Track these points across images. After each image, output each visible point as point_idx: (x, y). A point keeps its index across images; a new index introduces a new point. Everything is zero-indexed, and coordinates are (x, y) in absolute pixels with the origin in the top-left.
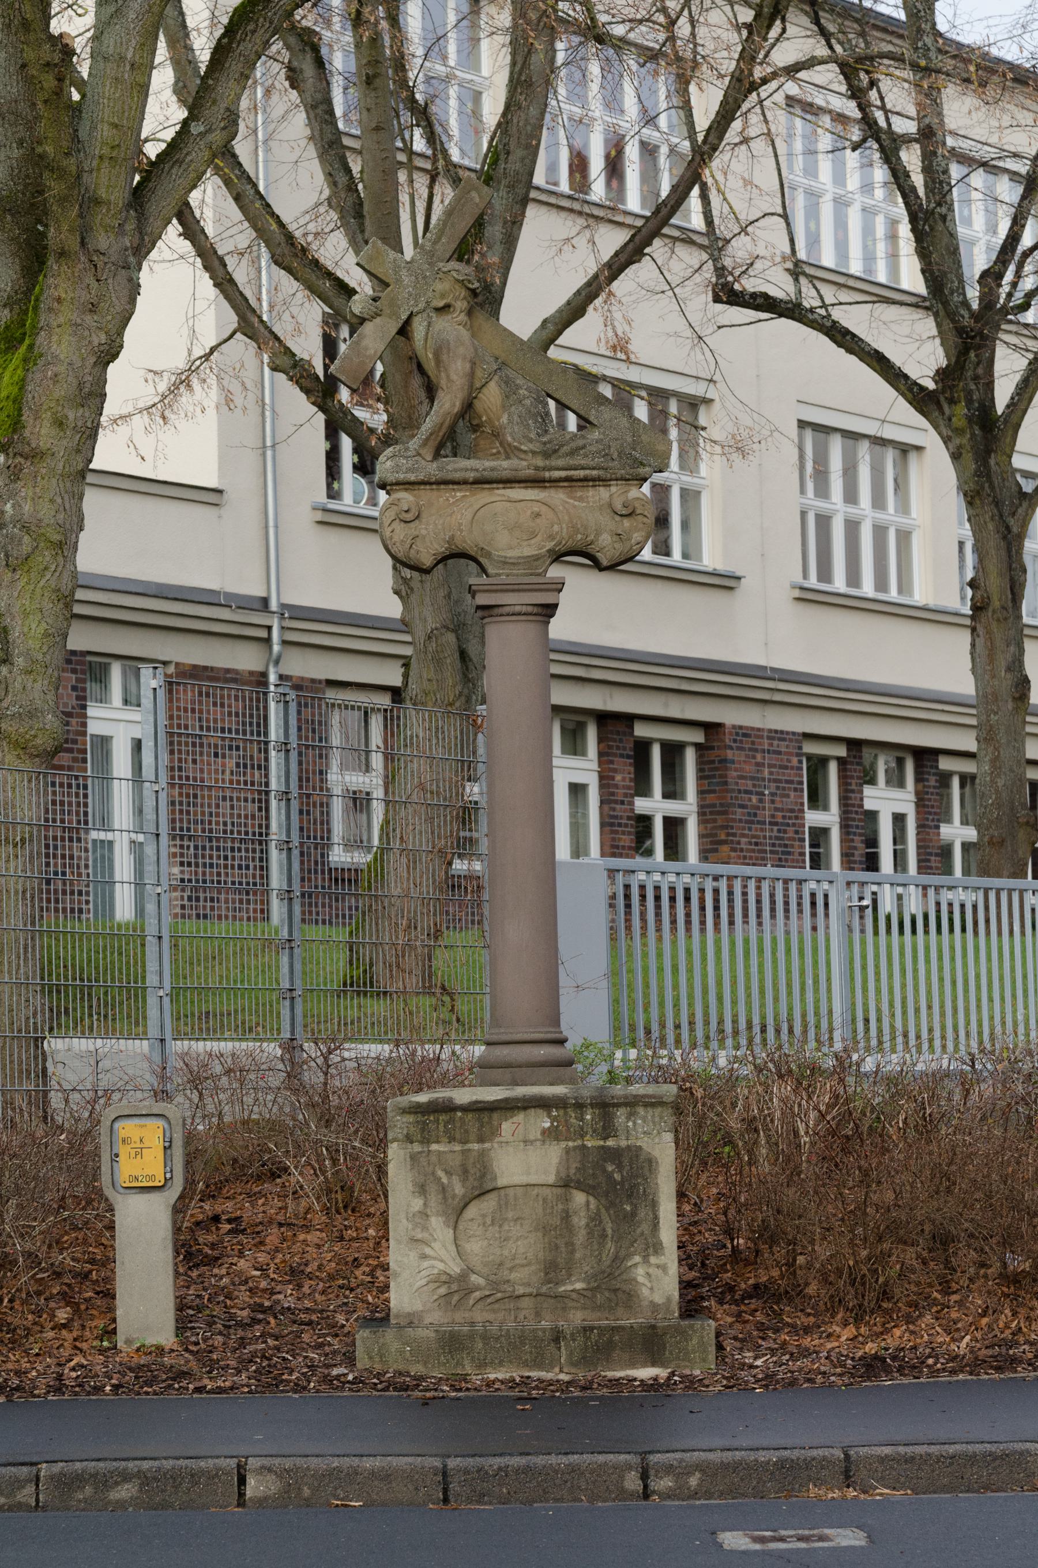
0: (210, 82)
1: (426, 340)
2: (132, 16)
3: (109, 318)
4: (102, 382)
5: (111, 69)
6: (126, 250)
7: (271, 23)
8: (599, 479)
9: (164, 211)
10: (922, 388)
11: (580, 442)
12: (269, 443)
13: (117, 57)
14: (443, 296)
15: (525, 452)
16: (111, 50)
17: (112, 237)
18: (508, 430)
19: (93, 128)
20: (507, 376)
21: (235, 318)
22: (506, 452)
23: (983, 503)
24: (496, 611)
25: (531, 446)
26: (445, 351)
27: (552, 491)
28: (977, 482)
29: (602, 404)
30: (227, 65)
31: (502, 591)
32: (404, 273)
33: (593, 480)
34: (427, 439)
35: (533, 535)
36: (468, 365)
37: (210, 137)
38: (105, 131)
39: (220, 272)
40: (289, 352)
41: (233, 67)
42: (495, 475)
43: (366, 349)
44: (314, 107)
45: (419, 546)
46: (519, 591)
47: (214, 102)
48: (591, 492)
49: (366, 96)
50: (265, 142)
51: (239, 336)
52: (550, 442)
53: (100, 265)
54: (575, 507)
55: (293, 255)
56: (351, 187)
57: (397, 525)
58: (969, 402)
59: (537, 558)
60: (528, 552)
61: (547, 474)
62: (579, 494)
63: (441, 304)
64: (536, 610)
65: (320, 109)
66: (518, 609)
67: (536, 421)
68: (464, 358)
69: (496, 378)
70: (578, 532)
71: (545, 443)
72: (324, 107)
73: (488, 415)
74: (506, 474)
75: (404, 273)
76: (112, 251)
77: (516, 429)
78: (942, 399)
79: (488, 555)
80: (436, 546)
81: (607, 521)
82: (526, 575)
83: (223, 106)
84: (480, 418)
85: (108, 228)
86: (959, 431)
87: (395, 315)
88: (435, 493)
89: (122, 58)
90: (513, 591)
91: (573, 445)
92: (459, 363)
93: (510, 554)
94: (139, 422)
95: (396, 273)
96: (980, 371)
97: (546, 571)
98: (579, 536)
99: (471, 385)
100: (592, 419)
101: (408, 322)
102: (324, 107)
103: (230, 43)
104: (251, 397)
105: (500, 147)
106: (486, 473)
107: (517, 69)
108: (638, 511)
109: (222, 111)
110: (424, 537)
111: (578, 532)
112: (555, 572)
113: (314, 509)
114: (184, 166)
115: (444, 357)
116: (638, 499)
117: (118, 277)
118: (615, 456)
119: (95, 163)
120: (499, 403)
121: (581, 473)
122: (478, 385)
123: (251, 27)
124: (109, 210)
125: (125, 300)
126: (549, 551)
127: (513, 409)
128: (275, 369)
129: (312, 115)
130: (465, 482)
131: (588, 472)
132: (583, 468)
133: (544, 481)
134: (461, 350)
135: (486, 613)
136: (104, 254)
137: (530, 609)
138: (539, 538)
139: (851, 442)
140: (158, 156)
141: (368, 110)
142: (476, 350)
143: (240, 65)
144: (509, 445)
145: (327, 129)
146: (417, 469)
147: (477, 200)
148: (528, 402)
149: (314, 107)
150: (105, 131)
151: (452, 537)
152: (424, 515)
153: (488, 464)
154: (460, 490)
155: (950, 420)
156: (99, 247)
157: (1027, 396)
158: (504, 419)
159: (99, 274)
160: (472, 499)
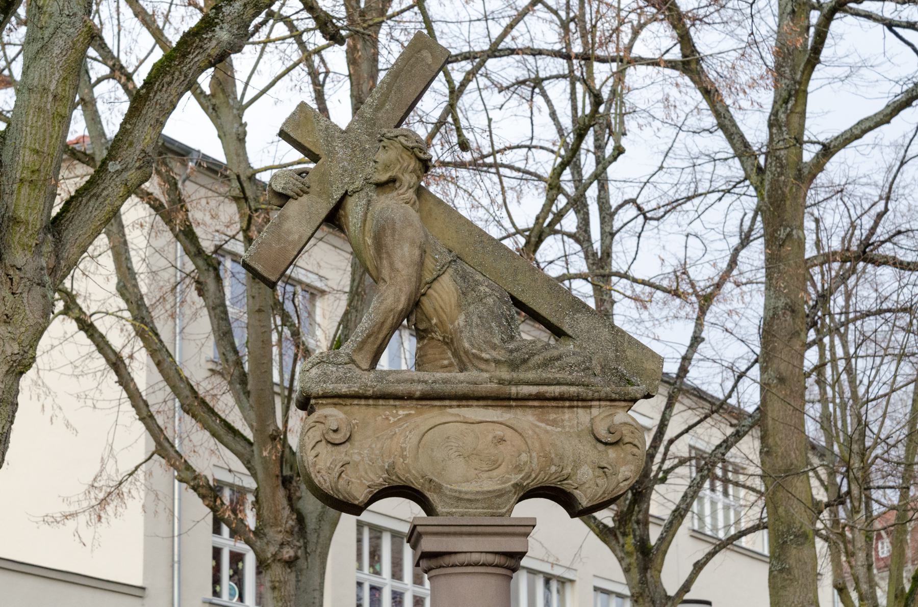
0: (128, 126)
1: (364, 221)
2: (57, 51)
3: (23, 329)
4: (14, 392)
5: (35, 100)
6: (42, 269)
7: (186, 76)
8: (579, 398)
9: (80, 240)
10: (605, 526)
11: (556, 353)
12: (176, 533)
13: (41, 89)
14: (387, 167)
15: (487, 361)
16: (35, 82)
17: (29, 256)
18: (466, 334)
19: (16, 153)
20: (464, 270)
21: (154, 444)
22: (461, 361)
23: (644, 601)
24: (448, 560)
25: (494, 354)
26: (389, 232)
27: (519, 412)
28: (641, 588)
29: (578, 311)
30: (144, 112)
31: (455, 534)
32: (338, 144)
33: (571, 399)
34: (364, 342)
35: (495, 464)
36: (417, 252)
37: (126, 175)
38: (26, 157)
39: (144, 410)
40: (188, 467)
41: (150, 114)
42: (448, 389)
43: (289, 233)
44: (214, 309)
45: (350, 474)
46: (476, 534)
47: (131, 144)
48: (567, 415)
49: (251, 288)
50: (181, 332)
51: (156, 456)
52: (517, 350)
53: (16, 279)
54: (547, 432)
55: (198, 407)
56: (239, 363)
57: (323, 448)
58: (635, 536)
59: (500, 494)
60: (489, 485)
61: (514, 390)
62: (552, 416)
63: (384, 177)
64: (498, 560)
65: (219, 312)
66: (475, 557)
67: (500, 325)
68: (413, 243)
69: (450, 271)
70: (552, 462)
71: (511, 351)
72: (222, 308)
73: (439, 317)
74: (463, 388)
75: (338, 144)
76: (27, 268)
77: (476, 332)
78: (618, 533)
79: (438, 489)
80: (372, 476)
81: (589, 452)
82: (485, 514)
83: (139, 148)
84: (429, 320)
85: (25, 247)
86: (629, 554)
87: (324, 193)
88: (372, 410)
89: (45, 90)
90: (470, 534)
91: (548, 354)
92: (406, 248)
93: (465, 487)
94: (83, 519)
95: (328, 144)
96: (640, 517)
97: (510, 511)
98: (553, 469)
99: (420, 278)
100: (566, 328)
101: (340, 205)
102: (222, 308)
103: (148, 93)
104: (161, 506)
105: (342, 337)
106: (436, 386)
107: (356, 284)
108: (627, 440)
109: (138, 152)
110: (357, 464)
111: (552, 462)
112: (526, 509)
113: (204, 602)
114: (101, 200)
115: (388, 240)
116: (625, 424)
117: (33, 293)
118: (598, 370)
119: (15, 186)
120: (454, 301)
121: (556, 390)
122: (428, 277)
123: (168, 79)
124: (26, 230)
125: (38, 314)
126: (516, 485)
127: (471, 308)
128: (180, 481)
129: (213, 314)
130: (410, 397)
131: (564, 389)
132: (559, 384)
133: (509, 399)
134: (409, 232)
135: (433, 563)
136: (20, 269)
137: (490, 558)
138: (502, 469)
139: (532, 576)
140: (77, 191)
141: (253, 297)
142: (426, 236)
143: (156, 113)
144: (466, 352)
145: (223, 323)
146: (350, 379)
147: (430, 60)
148: (490, 301)
149: (214, 309)
150: (26, 157)
151: (393, 465)
152: (357, 437)
153: (439, 375)
154: (403, 407)
155: (623, 546)
156: (16, 263)
157: (671, 533)
158: (461, 320)
159: (15, 288)
160: (419, 419)
